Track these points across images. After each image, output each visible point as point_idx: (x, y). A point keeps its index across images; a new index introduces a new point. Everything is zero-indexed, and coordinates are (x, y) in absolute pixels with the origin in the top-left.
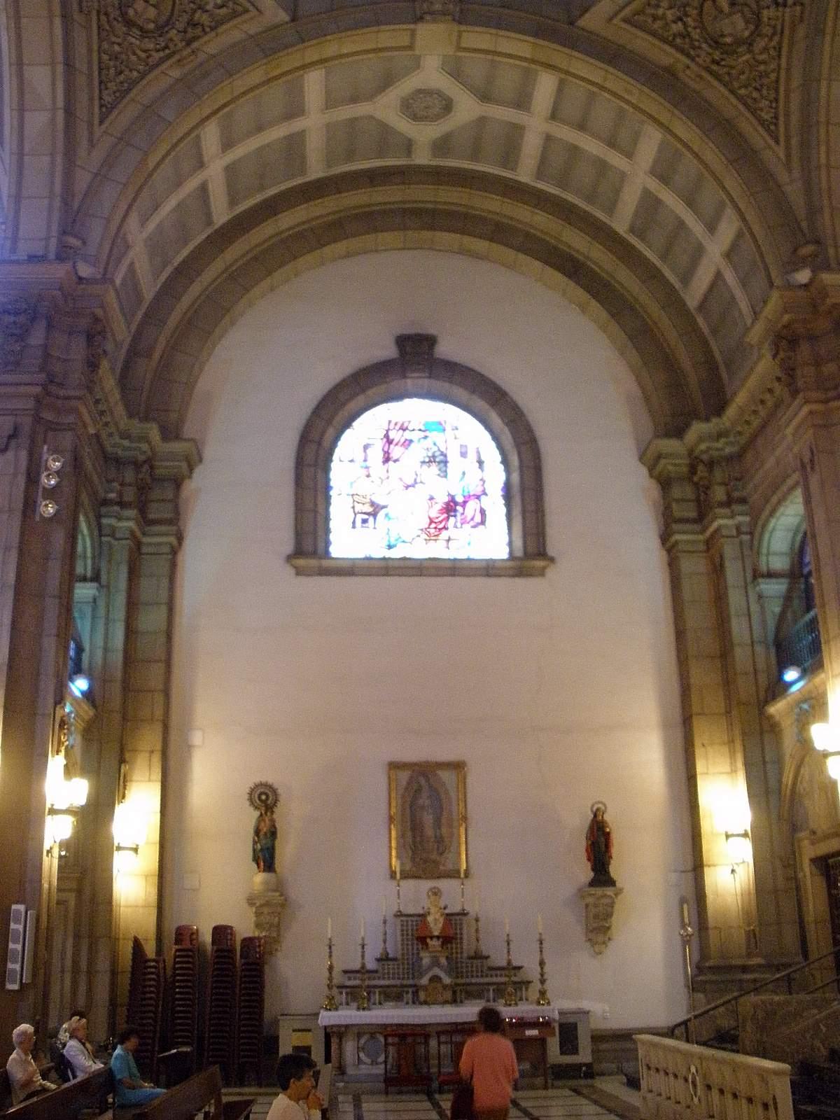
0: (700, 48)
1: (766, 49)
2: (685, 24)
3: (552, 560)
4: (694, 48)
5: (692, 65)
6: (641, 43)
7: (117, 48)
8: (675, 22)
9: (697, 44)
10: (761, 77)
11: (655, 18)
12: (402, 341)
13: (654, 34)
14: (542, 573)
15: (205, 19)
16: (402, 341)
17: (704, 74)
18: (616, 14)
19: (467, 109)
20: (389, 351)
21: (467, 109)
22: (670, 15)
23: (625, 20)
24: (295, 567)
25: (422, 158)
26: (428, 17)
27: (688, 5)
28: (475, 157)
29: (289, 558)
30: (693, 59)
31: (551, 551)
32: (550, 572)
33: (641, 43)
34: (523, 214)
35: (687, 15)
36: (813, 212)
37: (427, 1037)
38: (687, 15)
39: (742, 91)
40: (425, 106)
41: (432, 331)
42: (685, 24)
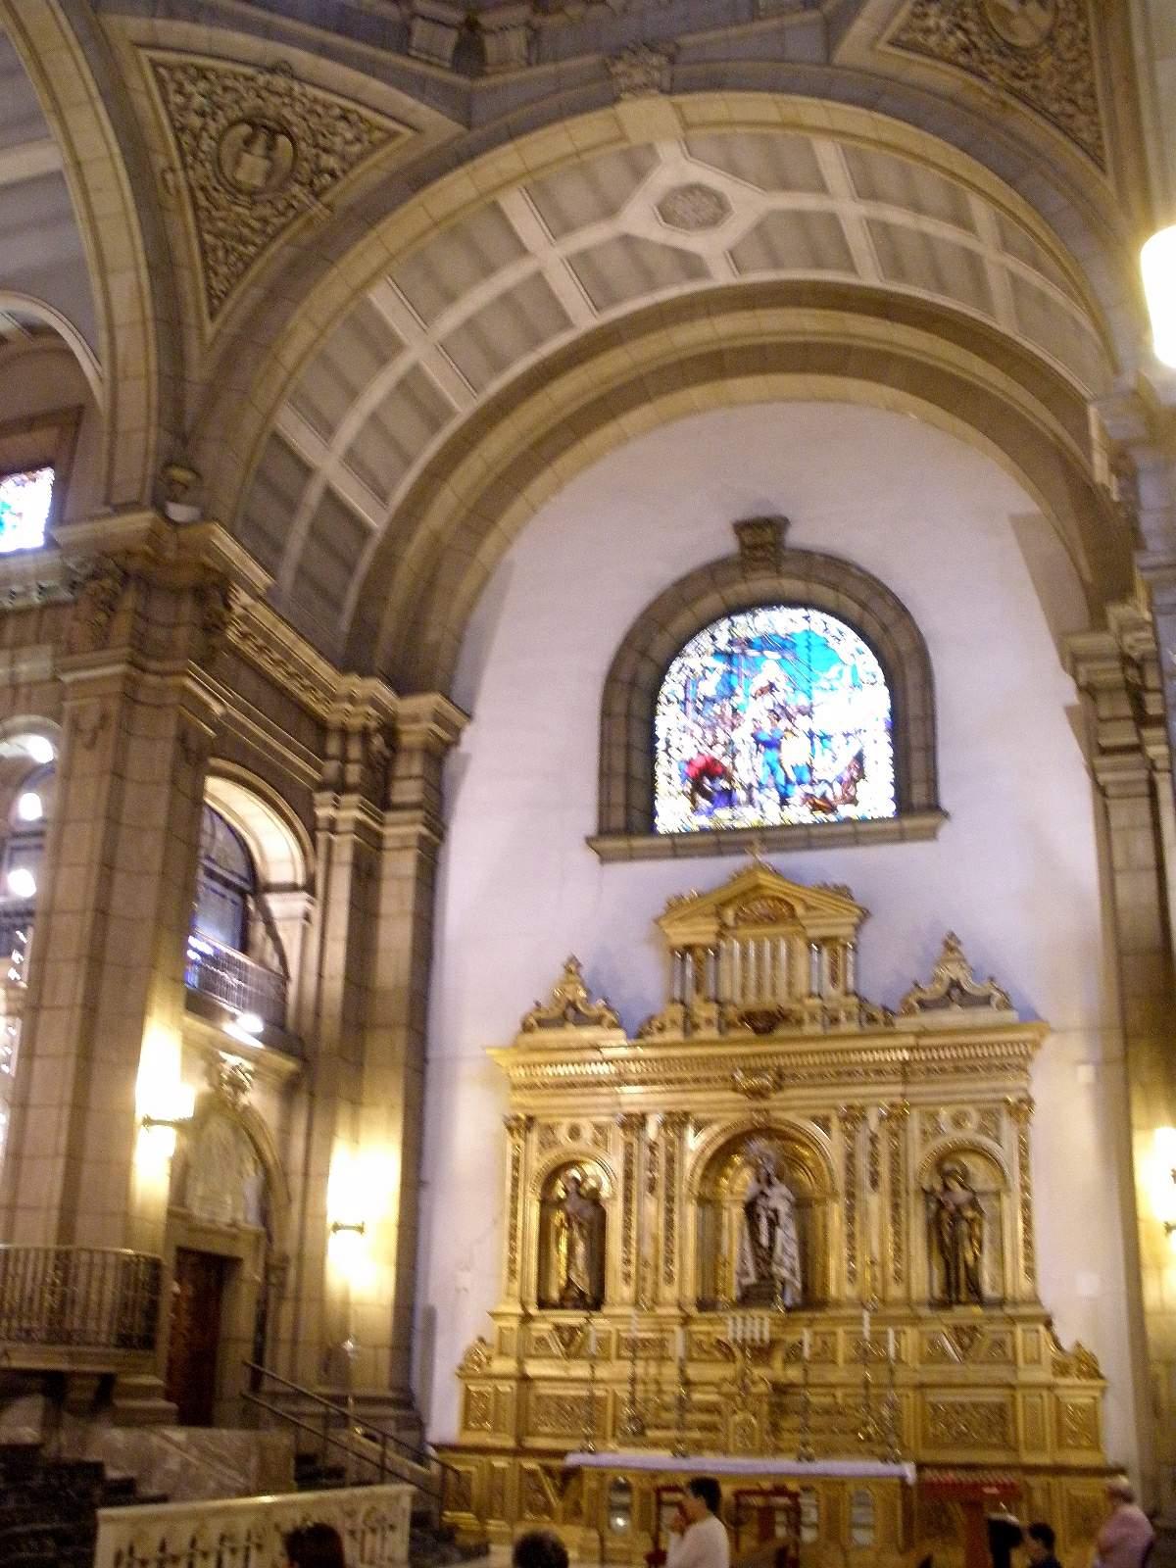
0: (991, 62)
1: (1072, 43)
2: (966, 32)
3: (946, 815)
4: (195, 156)
5: (181, 174)
6: (922, 71)
7: (221, 224)
8: (951, 33)
9: (987, 56)
10: (1073, 81)
11: (180, 91)
12: (742, 527)
13: (929, 53)
14: (931, 834)
15: (330, 162)
16: (742, 527)
17: (185, 194)
18: (877, 38)
19: (638, 218)
20: (727, 544)
21: (638, 218)
22: (198, 101)
23: (155, 65)
24: (598, 852)
25: (722, 276)
26: (626, 96)
27: (962, 4)
28: (652, 285)
29: (589, 841)
30: (185, 167)
31: (946, 802)
32: (946, 830)
33: (922, 71)
34: (614, 364)
35: (965, 17)
36: (212, 395)
37: (843, 1484)
38: (965, 17)
39: (208, 238)
40: (697, 206)
41: (786, 511)
42: (966, 32)
